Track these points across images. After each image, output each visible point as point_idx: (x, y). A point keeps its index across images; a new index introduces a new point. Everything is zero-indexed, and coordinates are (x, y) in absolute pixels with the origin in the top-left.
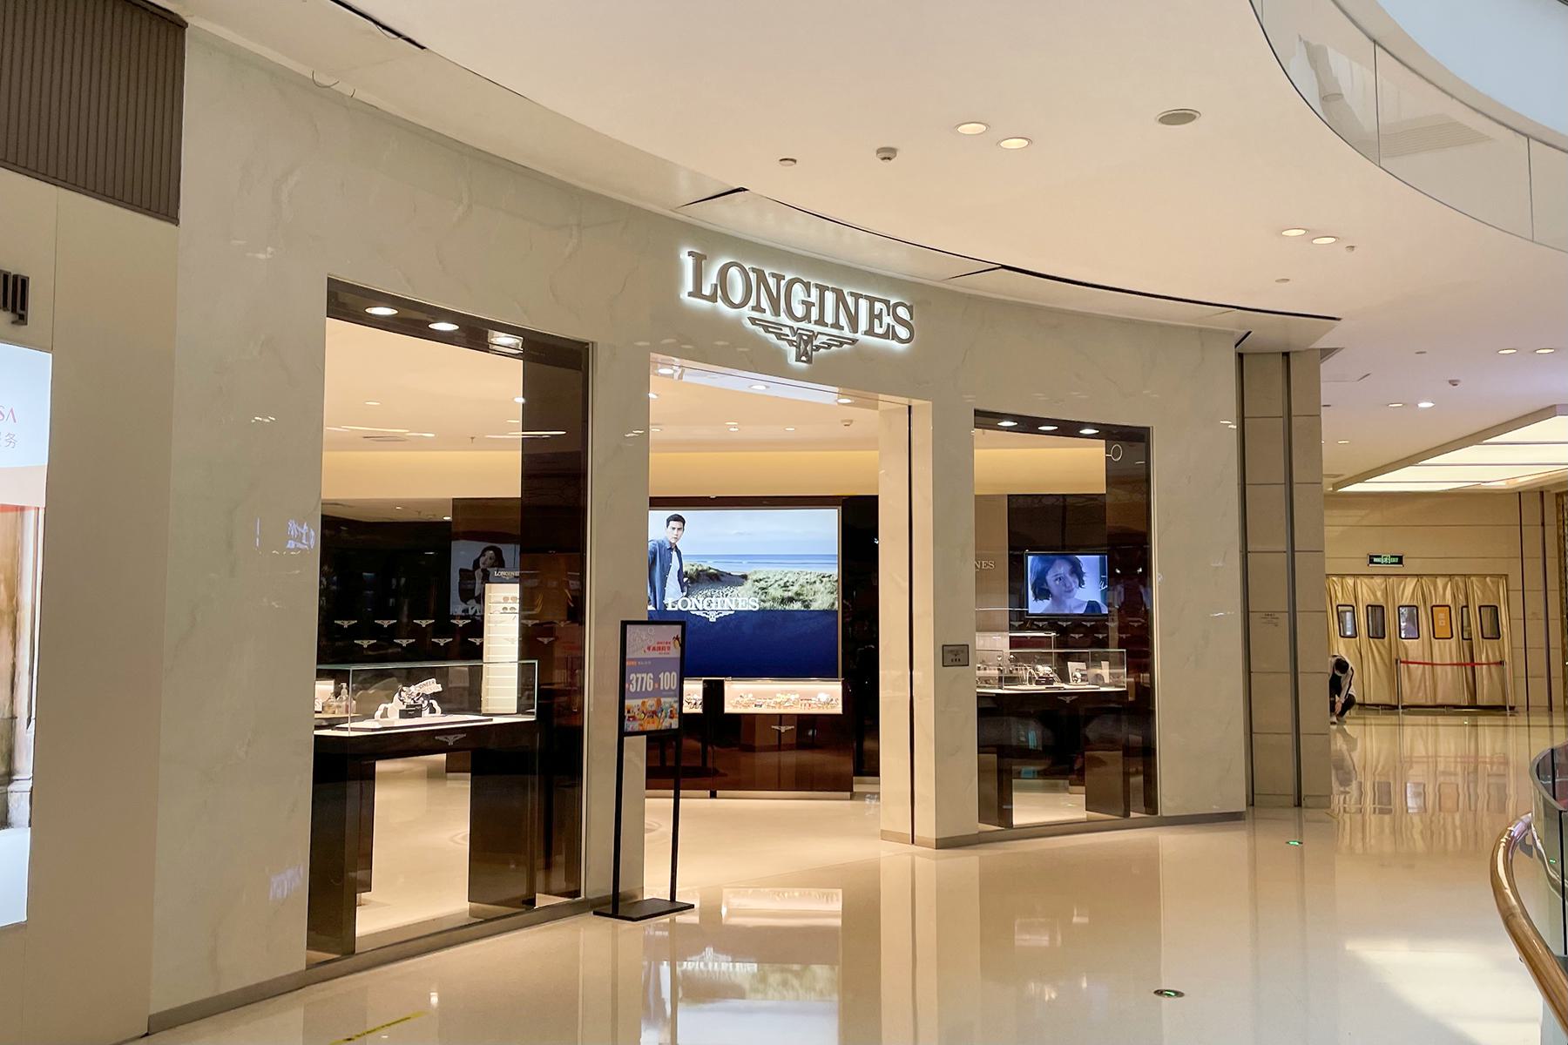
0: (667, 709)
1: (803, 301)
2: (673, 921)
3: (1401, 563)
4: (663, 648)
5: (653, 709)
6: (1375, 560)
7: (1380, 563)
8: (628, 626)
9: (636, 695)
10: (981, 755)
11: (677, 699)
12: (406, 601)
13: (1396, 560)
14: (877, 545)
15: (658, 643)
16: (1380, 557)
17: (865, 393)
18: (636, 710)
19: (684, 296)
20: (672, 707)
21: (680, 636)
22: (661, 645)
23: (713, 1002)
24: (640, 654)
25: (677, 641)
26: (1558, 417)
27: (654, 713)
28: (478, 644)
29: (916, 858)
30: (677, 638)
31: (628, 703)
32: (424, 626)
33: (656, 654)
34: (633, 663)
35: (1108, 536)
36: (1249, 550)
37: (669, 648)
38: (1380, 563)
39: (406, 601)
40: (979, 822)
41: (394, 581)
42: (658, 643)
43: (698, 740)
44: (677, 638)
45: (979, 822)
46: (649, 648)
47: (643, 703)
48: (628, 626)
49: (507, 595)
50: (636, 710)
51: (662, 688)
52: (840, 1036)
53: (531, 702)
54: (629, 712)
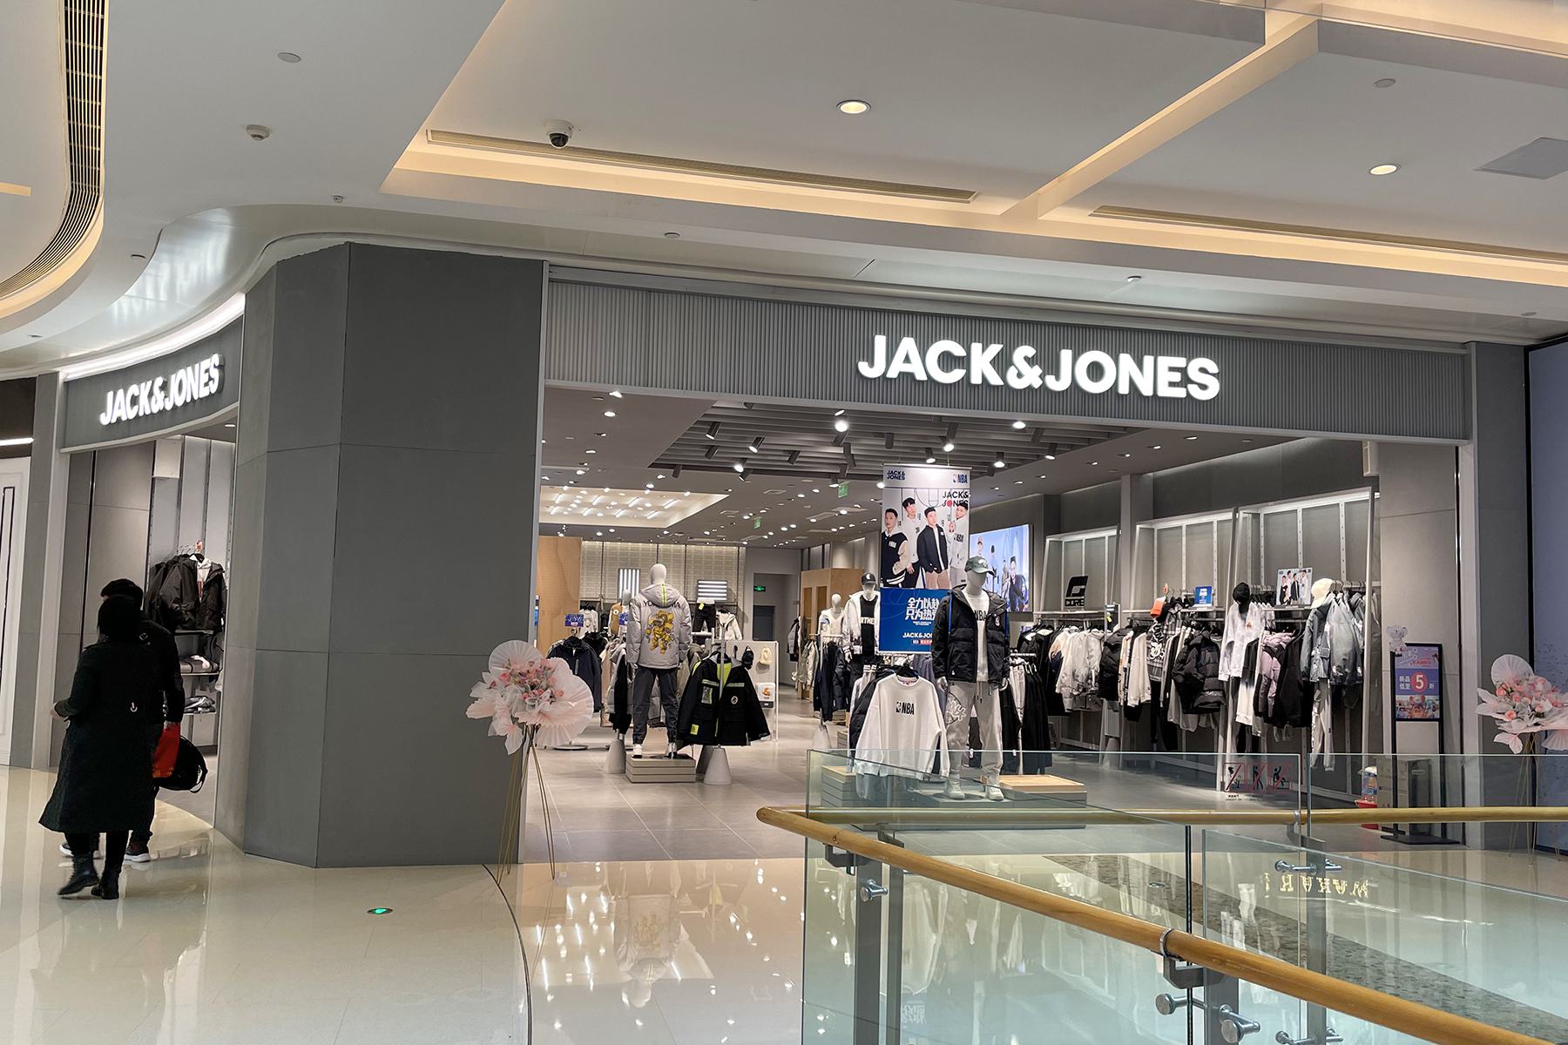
1: (1543, 717)
2: (960, 892)
4: (1426, 663)
5: (1419, 702)
9: (1405, 692)
11: (1438, 697)
12: (672, 964)
14: (944, 536)
18: (1405, 704)
26: (1098, 392)
27: (1420, 705)
28: (1015, 755)
30: (1436, 656)
31: (1398, 698)
32: (866, 667)
35: (118, 897)
39: (672, 964)
41: (713, 987)
44: (1436, 656)
47: (1411, 698)
50: (1405, 704)
53: (1184, 757)
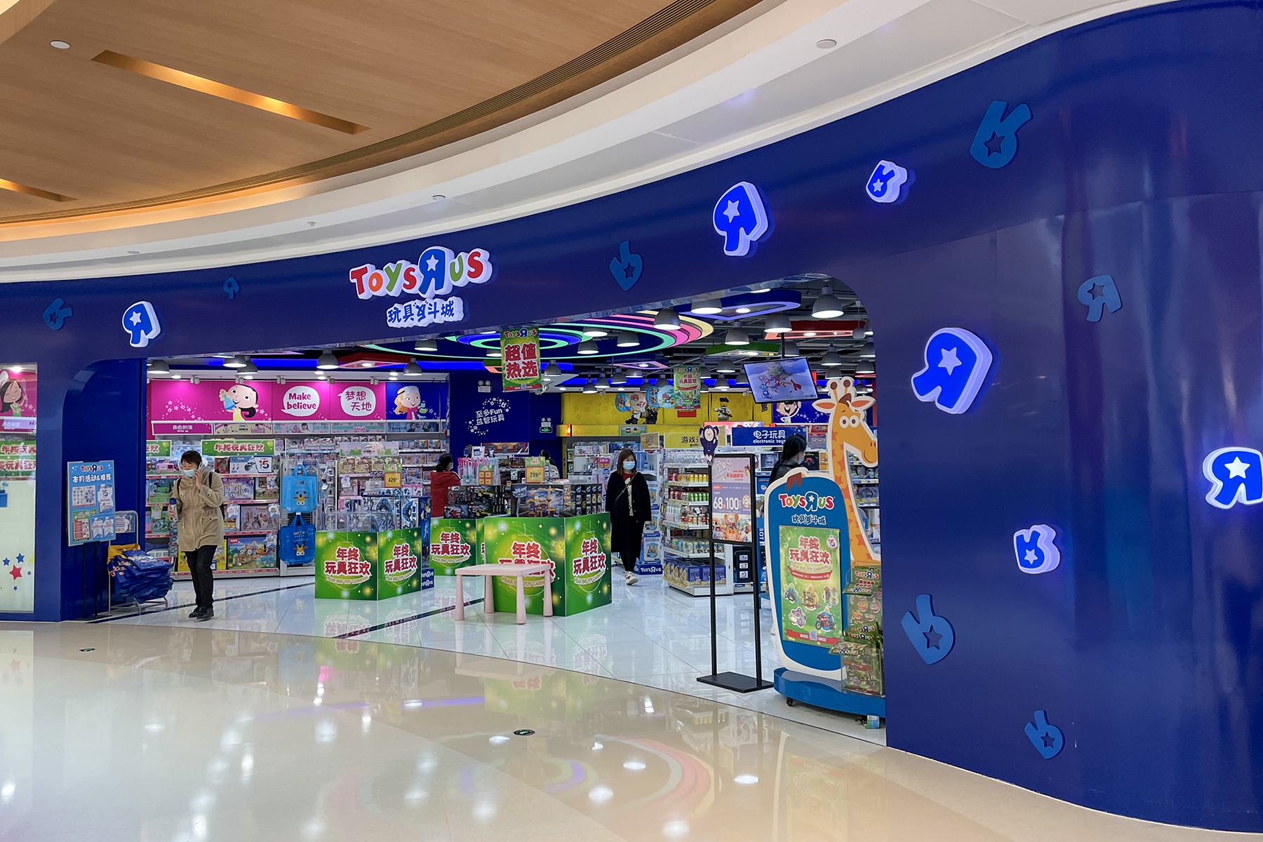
0: (743, 525)
4: (738, 476)
19: (761, 226)
20: (747, 524)
22: (737, 473)
23: (744, 136)
24: (724, 480)
27: (734, 525)
29: (482, 603)
30: (748, 467)
34: (717, 487)
36: (752, 596)
37: (742, 476)
40: (1040, 534)
43: (752, 773)
44: (748, 467)
45: (1040, 534)
46: (728, 476)
52: (839, 716)
54: (716, 524)
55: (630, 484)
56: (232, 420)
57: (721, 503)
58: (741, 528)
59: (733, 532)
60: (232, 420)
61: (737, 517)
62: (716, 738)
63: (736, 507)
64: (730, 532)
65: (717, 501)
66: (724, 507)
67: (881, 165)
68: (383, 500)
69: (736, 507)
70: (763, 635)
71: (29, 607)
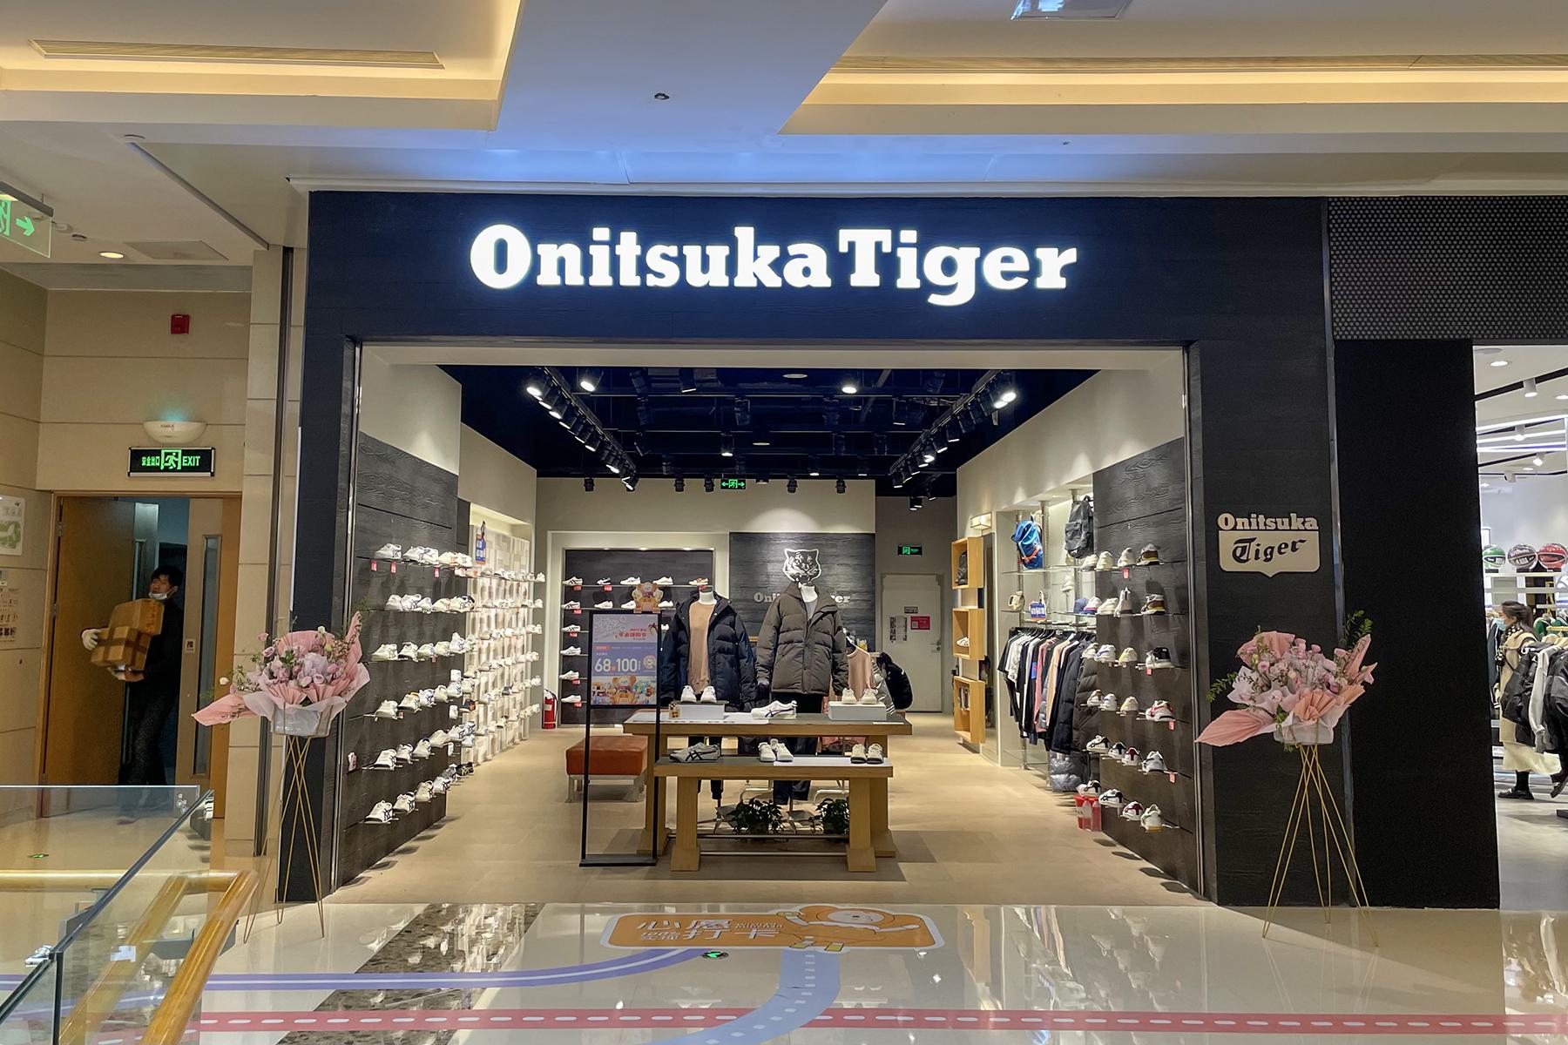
0: (642, 688)
3: (921, 554)
4: (638, 635)
6: (147, 461)
7: (157, 469)
8: (594, 615)
10: (878, 497)
13: (194, 461)
15: (632, 630)
16: (158, 453)
17: (1062, 952)
21: (656, 624)
25: (653, 629)
27: (628, 688)
30: (654, 626)
33: (630, 640)
38: (157, 469)
42: (632, 630)
48: (594, 615)
49: (1519, 681)
51: (619, 670)
55: (950, 445)
56: (1526, 578)
57: (609, 665)
58: (639, 690)
59: (650, 601)
60: (1526, 578)
61: (633, 680)
62: (1222, 530)
63: (633, 668)
64: (645, 601)
65: (601, 663)
66: (614, 668)
67: (727, 911)
68: (507, 568)
69: (633, 668)
70: (891, 801)
71: (192, 500)
